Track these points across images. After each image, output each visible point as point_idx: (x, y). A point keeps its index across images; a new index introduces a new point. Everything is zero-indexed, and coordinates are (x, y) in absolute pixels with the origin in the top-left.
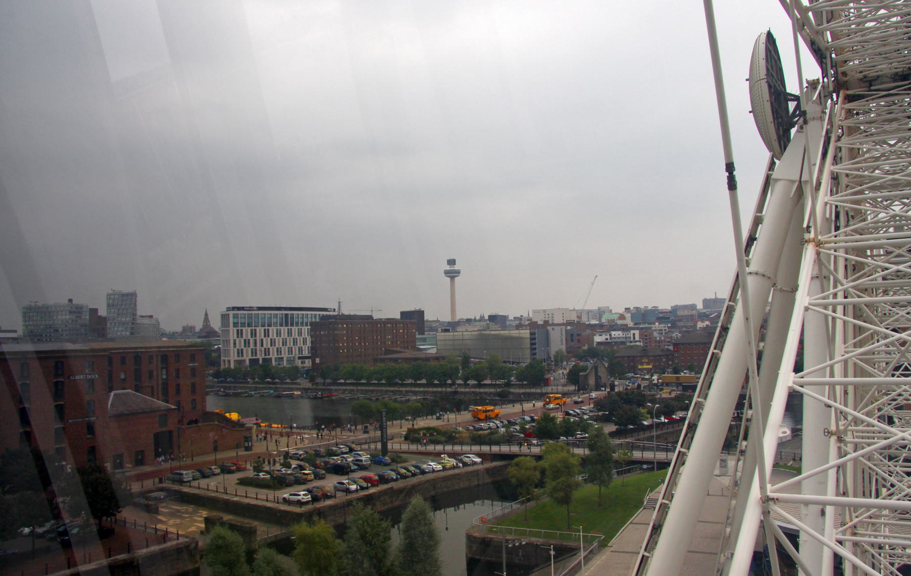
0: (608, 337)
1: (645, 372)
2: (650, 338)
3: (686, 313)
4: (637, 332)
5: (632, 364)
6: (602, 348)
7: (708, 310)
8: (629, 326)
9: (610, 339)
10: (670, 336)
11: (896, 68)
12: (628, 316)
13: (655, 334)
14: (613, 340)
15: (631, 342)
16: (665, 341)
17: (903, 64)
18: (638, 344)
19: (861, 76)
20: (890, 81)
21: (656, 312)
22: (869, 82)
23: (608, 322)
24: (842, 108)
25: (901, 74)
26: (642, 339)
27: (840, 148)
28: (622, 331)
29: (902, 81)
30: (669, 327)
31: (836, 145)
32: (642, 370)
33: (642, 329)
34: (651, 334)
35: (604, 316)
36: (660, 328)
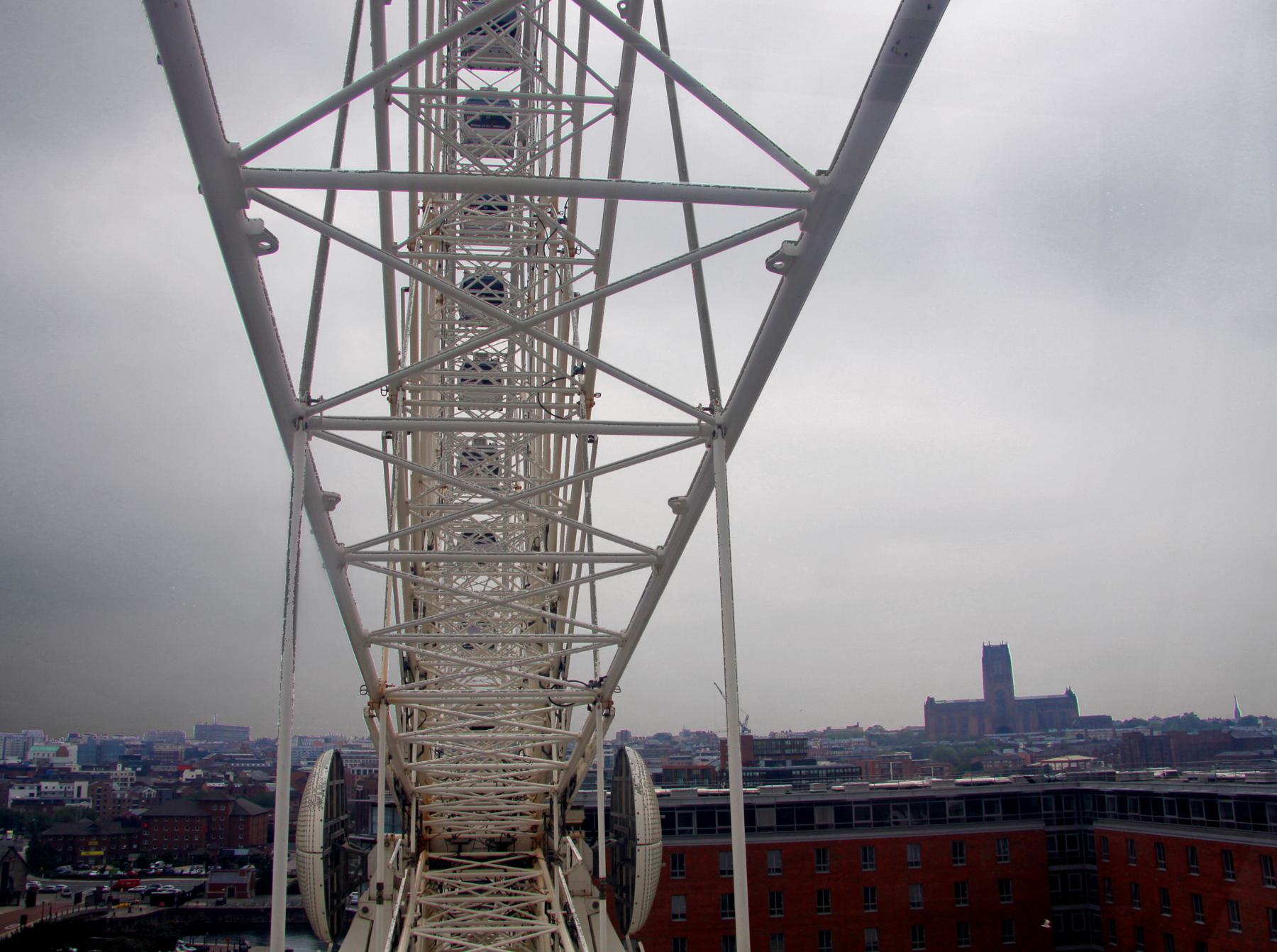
0: (35, 791)
1: (92, 861)
2: (105, 796)
3: (168, 748)
4: (85, 785)
5: (71, 848)
6: (22, 810)
7: (203, 742)
8: (73, 771)
9: (38, 794)
10: (138, 792)
11: (493, 833)
12: (73, 749)
13: (115, 786)
14: (45, 797)
15: (73, 801)
16: (129, 801)
17: (501, 829)
18: (84, 804)
19: (449, 835)
20: (484, 848)
21: (121, 745)
22: (459, 844)
23: (38, 762)
24: (423, 878)
25: (498, 840)
26: (92, 796)
27: (416, 937)
28: (60, 782)
29: (499, 850)
30: (138, 774)
31: (412, 933)
32: (86, 858)
33: (94, 777)
34: (108, 789)
35: (32, 749)
36: (124, 776)
